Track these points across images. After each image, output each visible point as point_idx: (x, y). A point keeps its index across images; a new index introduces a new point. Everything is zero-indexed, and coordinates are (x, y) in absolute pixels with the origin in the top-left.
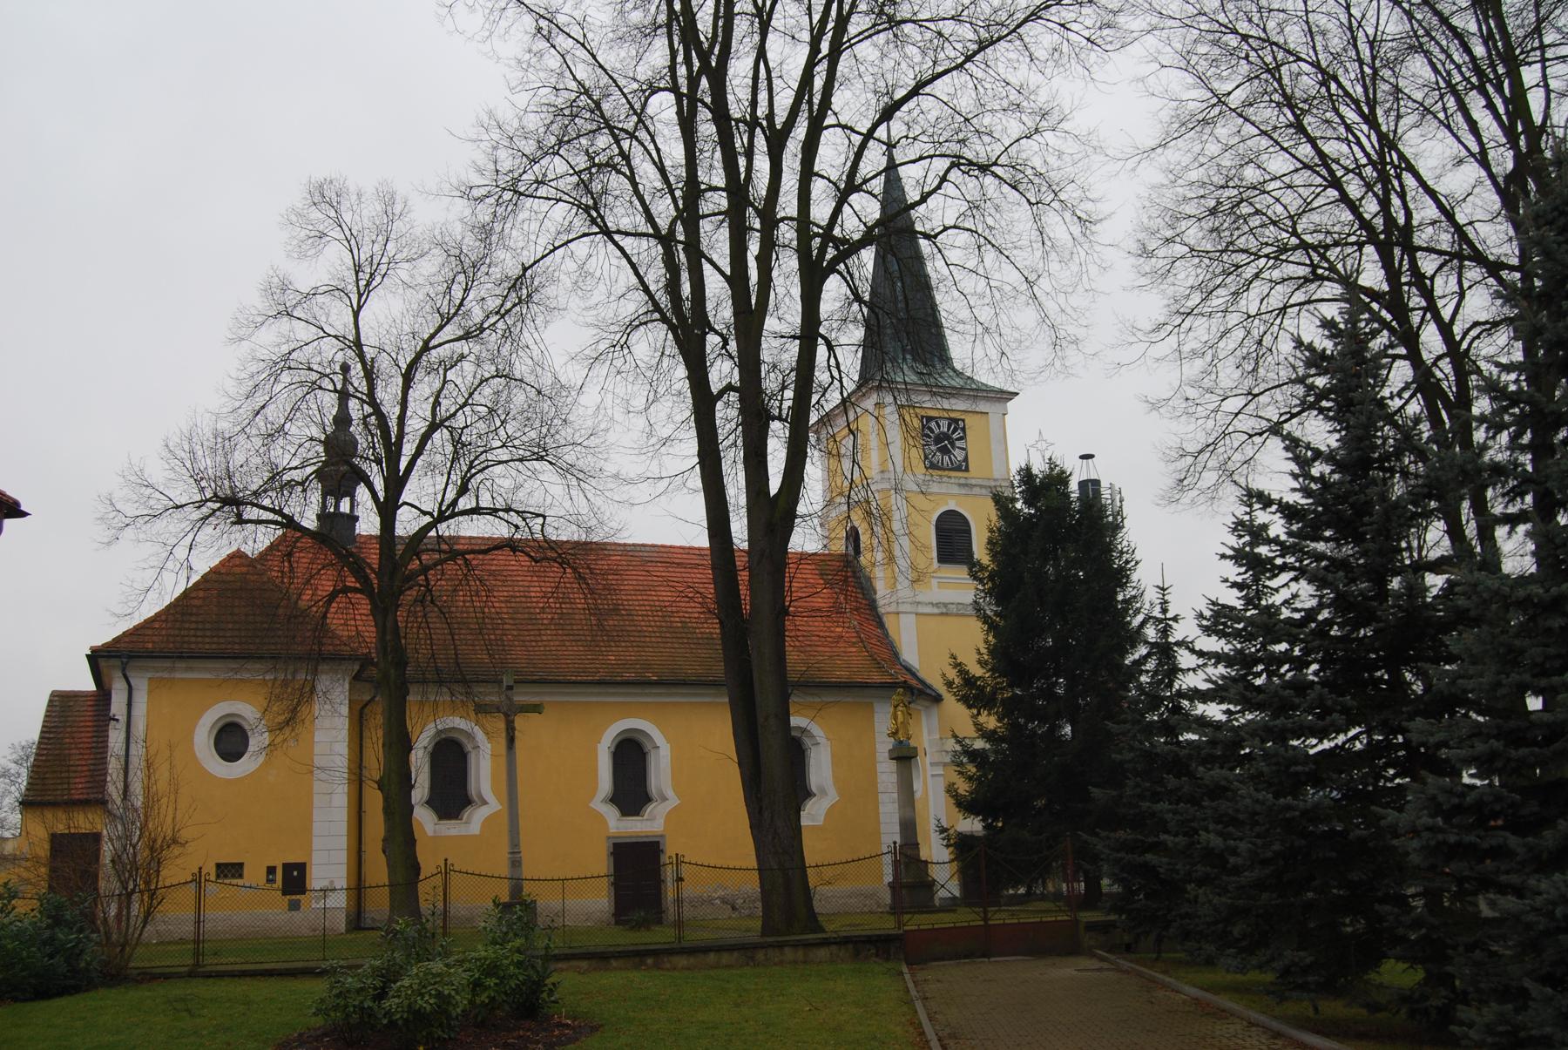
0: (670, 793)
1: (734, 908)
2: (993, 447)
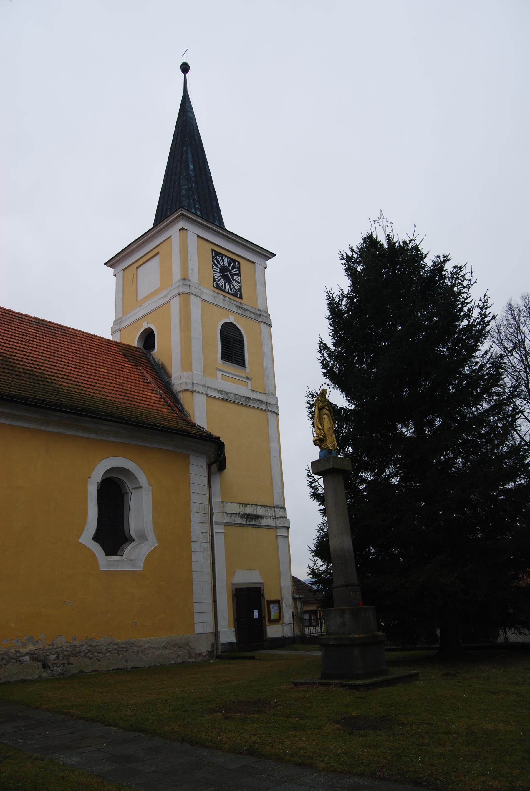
1: (45, 666)
2: (258, 287)
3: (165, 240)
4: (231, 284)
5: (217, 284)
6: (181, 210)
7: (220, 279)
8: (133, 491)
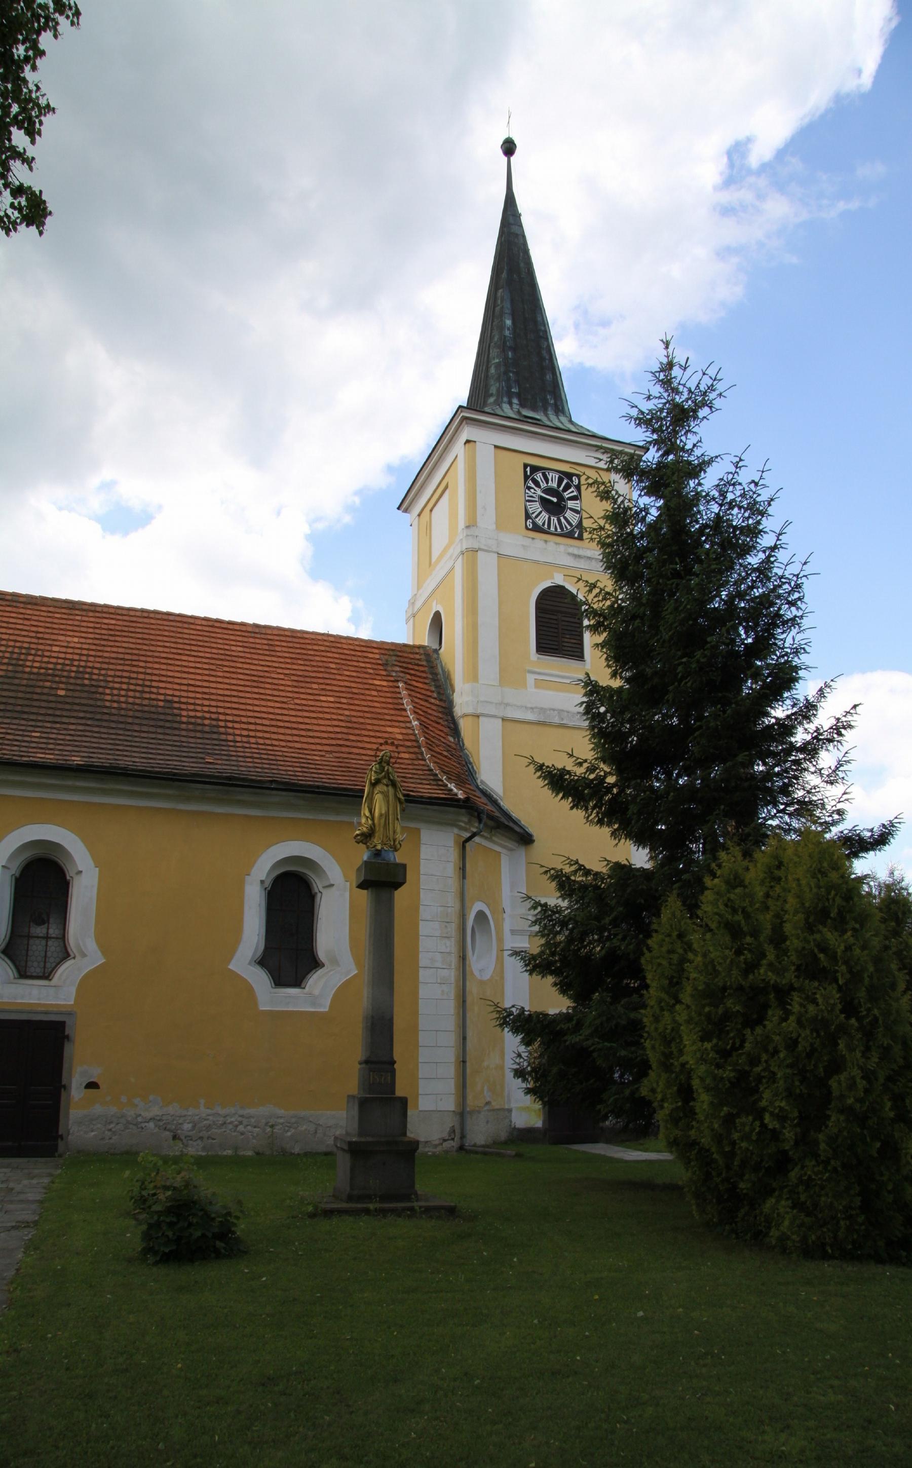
0: (91, 945)
3: (453, 463)
4: (562, 518)
5: (534, 523)
6: (461, 412)
7: (541, 512)
8: (324, 891)
